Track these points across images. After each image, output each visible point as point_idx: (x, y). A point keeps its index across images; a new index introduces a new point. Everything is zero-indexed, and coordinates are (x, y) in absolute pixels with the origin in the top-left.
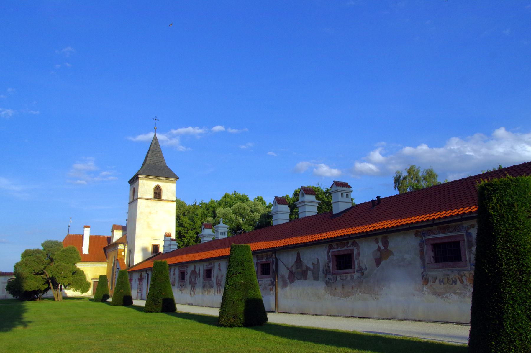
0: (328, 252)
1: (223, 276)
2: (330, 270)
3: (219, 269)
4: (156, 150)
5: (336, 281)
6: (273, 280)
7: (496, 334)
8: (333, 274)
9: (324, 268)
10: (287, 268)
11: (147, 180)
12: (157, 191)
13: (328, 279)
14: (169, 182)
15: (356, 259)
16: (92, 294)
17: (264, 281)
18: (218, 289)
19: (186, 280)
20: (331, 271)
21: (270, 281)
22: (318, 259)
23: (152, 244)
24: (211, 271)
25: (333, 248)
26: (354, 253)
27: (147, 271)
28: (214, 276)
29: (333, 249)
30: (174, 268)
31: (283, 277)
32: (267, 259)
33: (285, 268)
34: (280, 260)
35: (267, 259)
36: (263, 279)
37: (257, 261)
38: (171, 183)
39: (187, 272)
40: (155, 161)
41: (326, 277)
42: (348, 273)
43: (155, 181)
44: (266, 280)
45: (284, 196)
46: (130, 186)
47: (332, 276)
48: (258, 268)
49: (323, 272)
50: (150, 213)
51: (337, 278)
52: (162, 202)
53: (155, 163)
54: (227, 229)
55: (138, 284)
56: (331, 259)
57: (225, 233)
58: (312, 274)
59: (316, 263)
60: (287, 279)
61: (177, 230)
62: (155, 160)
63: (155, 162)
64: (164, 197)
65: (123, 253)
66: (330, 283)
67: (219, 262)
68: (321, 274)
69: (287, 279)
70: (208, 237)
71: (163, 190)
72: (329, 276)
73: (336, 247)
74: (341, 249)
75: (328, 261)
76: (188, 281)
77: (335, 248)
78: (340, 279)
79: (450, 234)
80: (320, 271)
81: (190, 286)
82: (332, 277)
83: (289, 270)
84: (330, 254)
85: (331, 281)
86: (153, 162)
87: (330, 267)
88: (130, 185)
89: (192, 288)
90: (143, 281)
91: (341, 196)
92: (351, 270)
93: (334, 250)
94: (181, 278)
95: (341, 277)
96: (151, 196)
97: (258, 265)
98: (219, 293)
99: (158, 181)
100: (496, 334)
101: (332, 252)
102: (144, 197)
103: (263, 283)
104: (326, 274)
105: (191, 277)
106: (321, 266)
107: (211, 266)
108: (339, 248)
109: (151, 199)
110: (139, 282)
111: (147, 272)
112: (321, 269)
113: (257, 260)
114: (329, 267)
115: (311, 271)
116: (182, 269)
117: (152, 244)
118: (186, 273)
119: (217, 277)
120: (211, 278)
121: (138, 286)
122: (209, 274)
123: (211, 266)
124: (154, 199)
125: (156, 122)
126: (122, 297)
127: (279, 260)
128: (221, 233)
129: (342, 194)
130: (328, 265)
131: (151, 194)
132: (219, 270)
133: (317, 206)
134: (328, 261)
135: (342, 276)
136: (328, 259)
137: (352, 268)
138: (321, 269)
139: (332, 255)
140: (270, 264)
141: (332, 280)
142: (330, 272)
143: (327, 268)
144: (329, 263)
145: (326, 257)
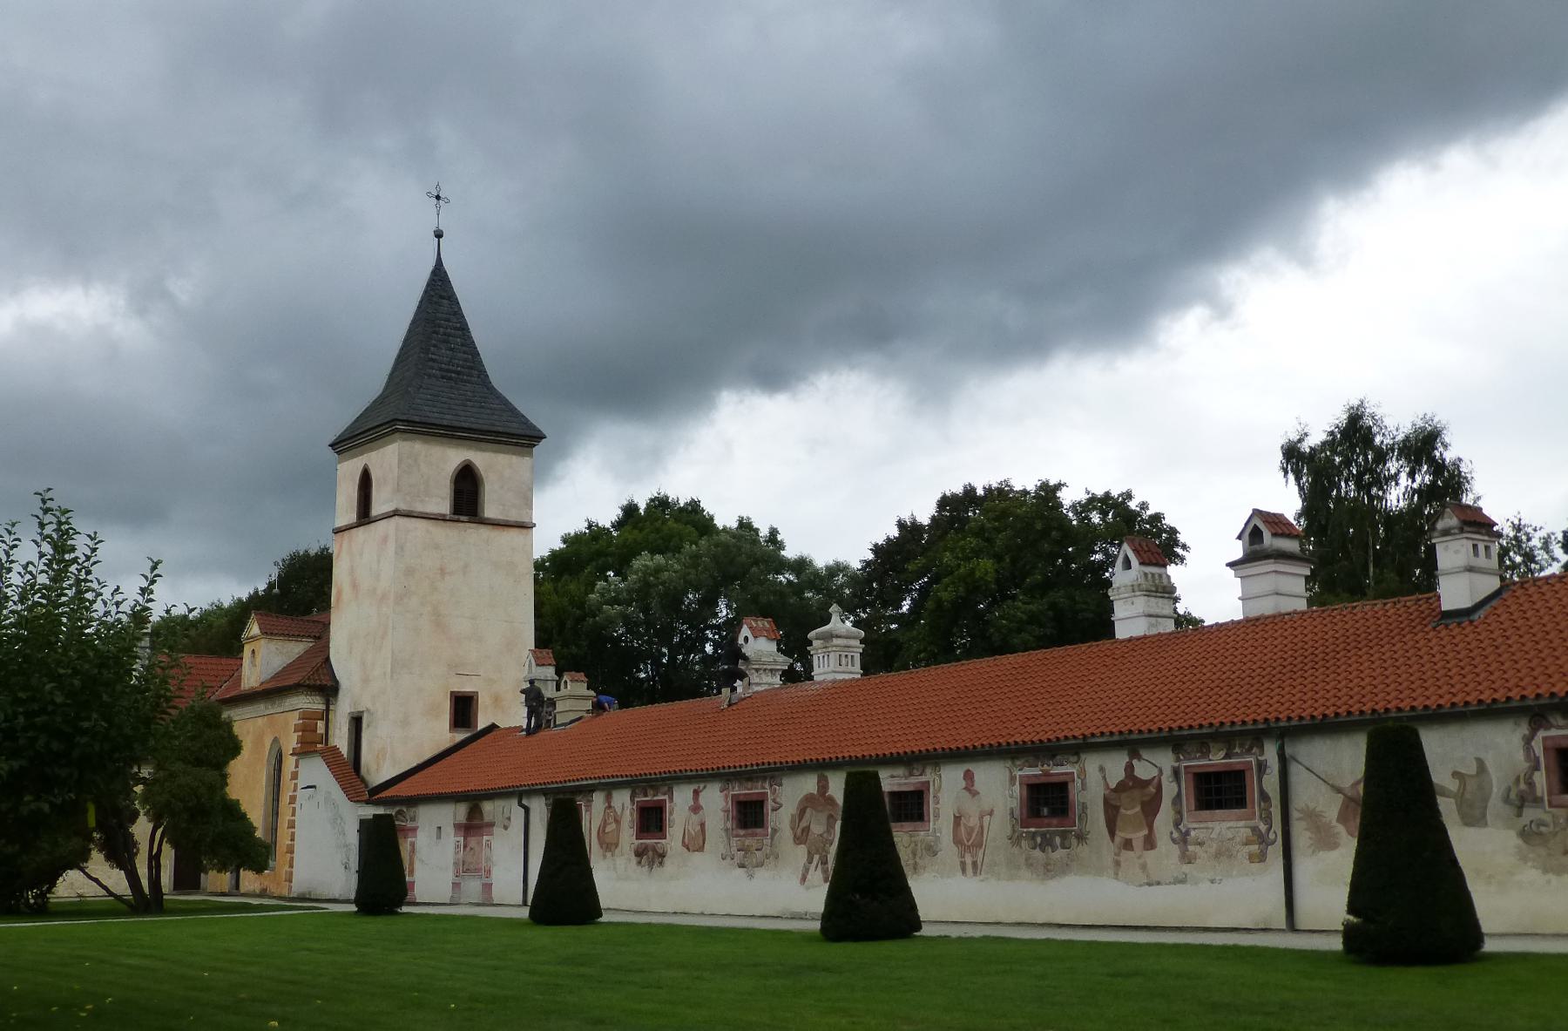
0: (1528, 741)
1: (991, 813)
2: (1539, 793)
4: (448, 320)
6: (1263, 827)
10: (1333, 786)
13: (1531, 822)
16: (172, 888)
18: (969, 860)
19: (775, 831)
20: (1542, 799)
23: (452, 693)
24: (762, 807)
28: (937, 816)
31: (1312, 816)
32: (1227, 756)
33: (1324, 787)
35: (1227, 756)
36: (1210, 825)
37: (1176, 764)
39: (774, 801)
40: (447, 367)
43: (458, 446)
44: (1229, 828)
47: (1549, 812)
52: (484, 532)
53: (449, 374)
54: (857, 643)
57: (852, 656)
58: (1454, 807)
59: (1472, 769)
61: (321, 617)
64: (490, 511)
65: (321, 725)
68: (1495, 803)
69: (1334, 823)
70: (765, 670)
75: (1527, 765)
76: (786, 833)
80: (1493, 796)
81: (802, 850)
82: (1547, 818)
83: (1344, 794)
84: (1538, 746)
85: (1543, 829)
86: (441, 369)
89: (810, 861)
91: (1472, 554)
94: (740, 820)
96: (445, 507)
98: (975, 873)
99: (470, 448)
102: (419, 508)
103: (1214, 836)
111: (525, 802)
112: (1495, 790)
113: (1178, 760)
114: (1531, 784)
115: (1448, 797)
116: (749, 790)
117: (452, 693)
118: (770, 804)
119: (957, 820)
121: (457, 853)
122: (750, 815)
125: (438, 208)
126: (1158, 845)
128: (840, 655)
130: (1531, 777)
132: (967, 794)
133: (1307, 578)
134: (1527, 765)
138: (1497, 791)
142: (1537, 801)
143: (1523, 786)
144: (1532, 774)
145: (1520, 755)
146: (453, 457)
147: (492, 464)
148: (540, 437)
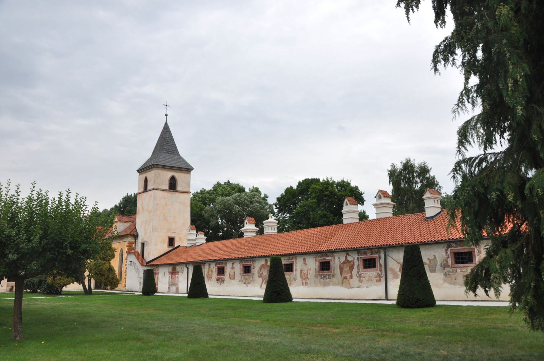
0: (446, 250)
3: (304, 263)
5: (455, 273)
7: (482, 9)
8: (452, 267)
9: (442, 263)
11: (162, 170)
12: (172, 182)
14: (179, 172)
15: (477, 256)
17: (368, 274)
19: (253, 274)
21: (376, 274)
22: (435, 256)
23: (168, 237)
24: (250, 268)
25: (452, 247)
26: (475, 251)
27: (187, 264)
28: (296, 270)
29: (451, 247)
30: (338, 257)
34: (389, 256)
38: (185, 173)
39: (253, 266)
41: (444, 270)
42: (469, 267)
45: (365, 199)
46: (139, 175)
48: (360, 262)
49: (441, 266)
50: (166, 204)
51: (457, 271)
52: (177, 194)
55: (169, 278)
56: (450, 255)
60: (398, 272)
62: (168, 148)
63: (168, 151)
64: (179, 188)
66: (450, 274)
67: (304, 257)
71: (178, 180)
72: (447, 269)
73: (455, 246)
74: (461, 248)
76: (256, 275)
77: (454, 247)
78: (461, 271)
79: (353, 208)
80: (438, 265)
82: (451, 270)
85: (450, 273)
87: (449, 262)
88: (138, 174)
90: (178, 274)
92: (472, 264)
93: (453, 248)
95: (461, 269)
96: (167, 187)
97: (360, 260)
99: (174, 172)
100: (482, 9)
101: (451, 250)
102: (160, 187)
104: (444, 268)
105: (260, 271)
106: (438, 261)
107: (292, 260)
108: (459, 247)
109: (166, 190)
110: (171, 276)
112: (438, 263)
114: (447, 262)
117: (168, 237)
119: (301, 271)
120: (292, 271)
123: (292, 260)
124: (170, 190)
127: (388, 256)
129: (437, 201)
131: (167, 185)
135: (462, 269)
136: (446, 255)
137: (474, 262)
139: (451, 253)
140: (376, 259)
141: (451, 272)
143: (445, 262)
146: (169, 174)
147: (178, 175)
148: (192, 169)
